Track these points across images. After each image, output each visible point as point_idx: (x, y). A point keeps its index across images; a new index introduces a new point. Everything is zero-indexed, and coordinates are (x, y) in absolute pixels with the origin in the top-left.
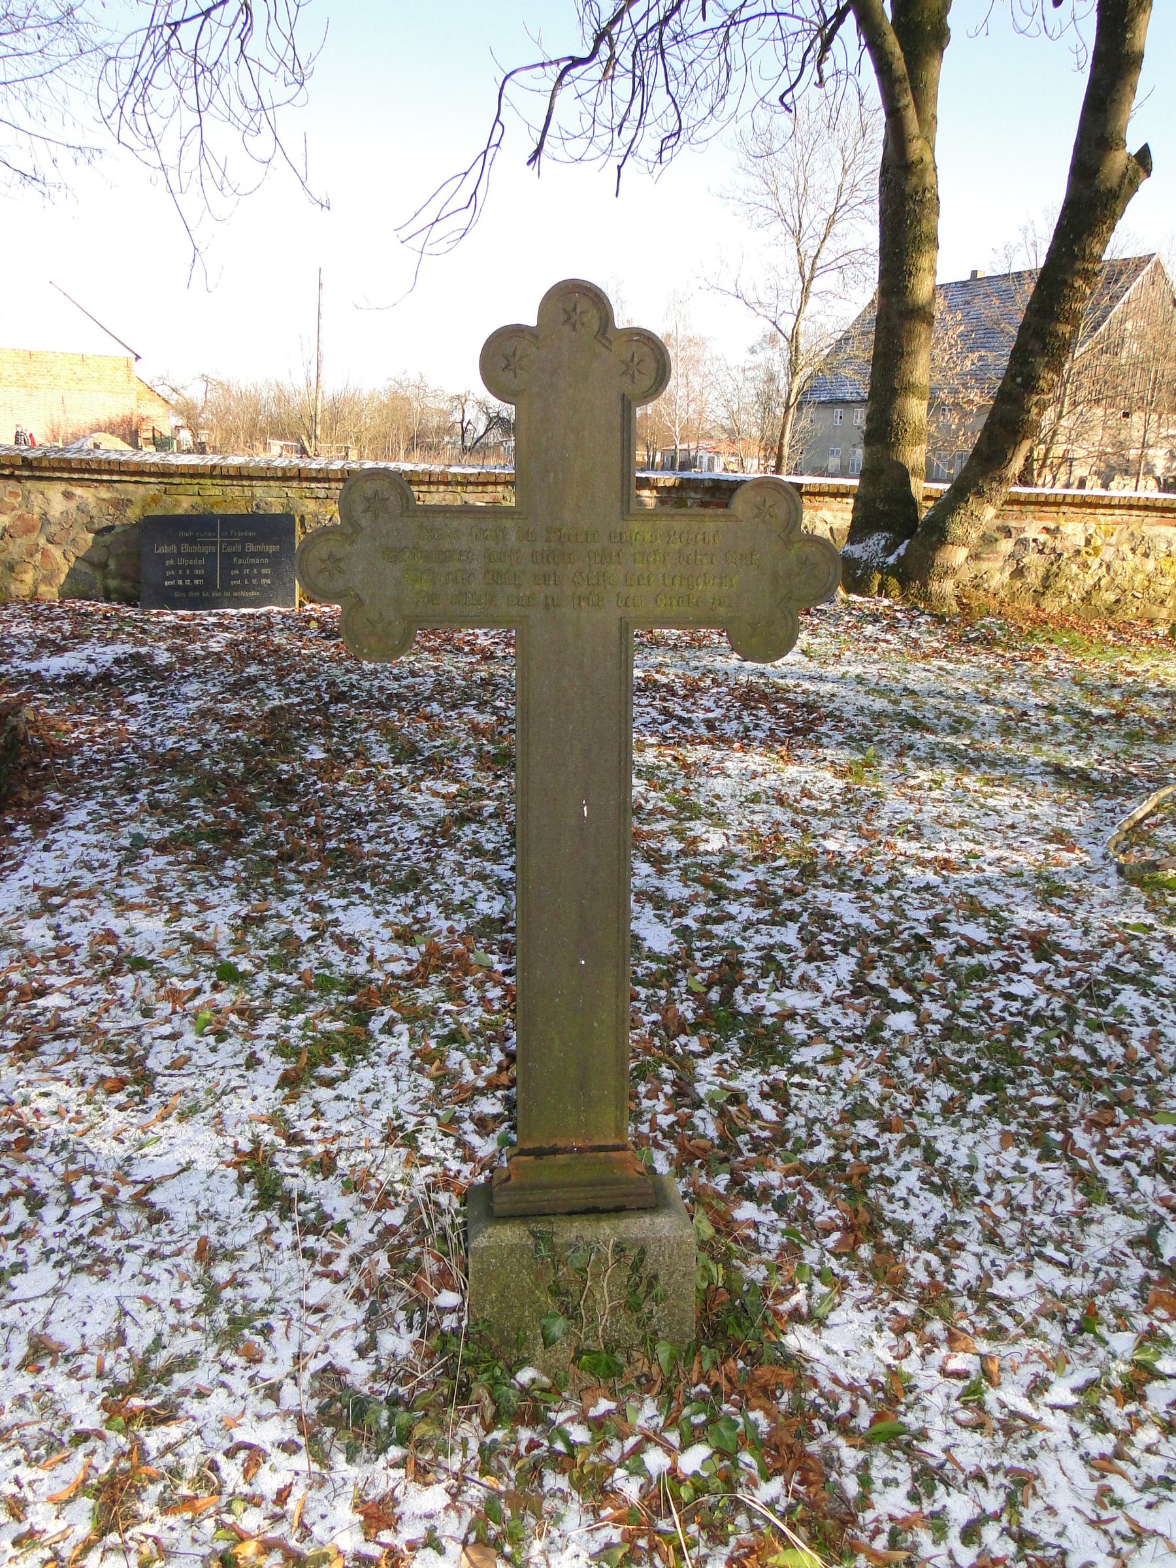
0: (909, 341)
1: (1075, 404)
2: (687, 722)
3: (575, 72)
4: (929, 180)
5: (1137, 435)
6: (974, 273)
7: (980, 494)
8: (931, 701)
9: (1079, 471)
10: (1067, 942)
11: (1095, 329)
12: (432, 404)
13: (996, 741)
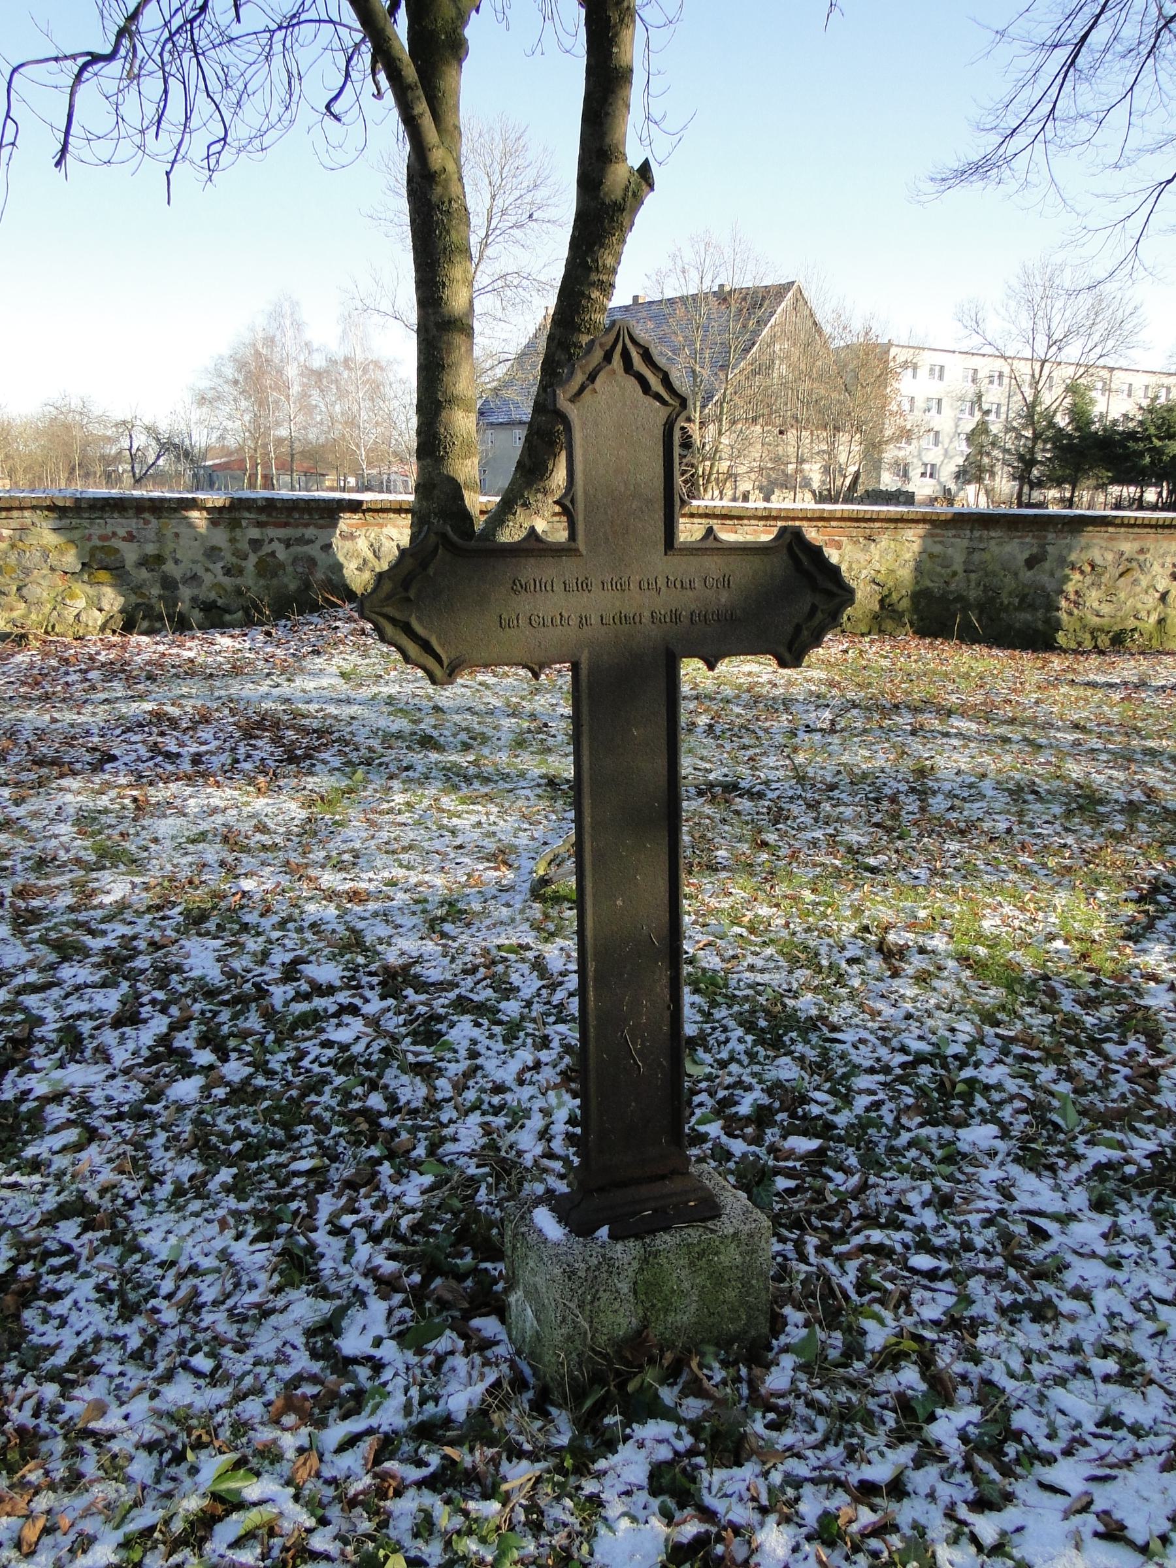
0: (449, 353)
1: (734, 422)
2: (170, 757)
3: (96, 67)
4: (454, 189)
5: (791, 450)
6: (636, 298)
7: (526, 505)
8: (457, 718)
9: (745, 486)
10: (431, 972)
11: (747, 350)
12: (98, 430)
13: (503, 757)
